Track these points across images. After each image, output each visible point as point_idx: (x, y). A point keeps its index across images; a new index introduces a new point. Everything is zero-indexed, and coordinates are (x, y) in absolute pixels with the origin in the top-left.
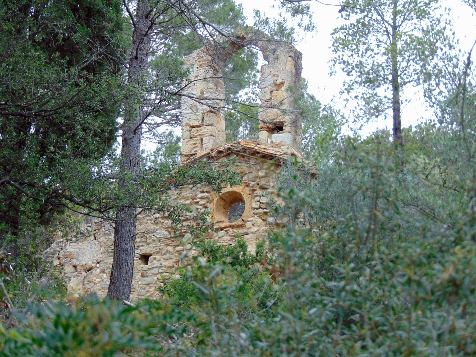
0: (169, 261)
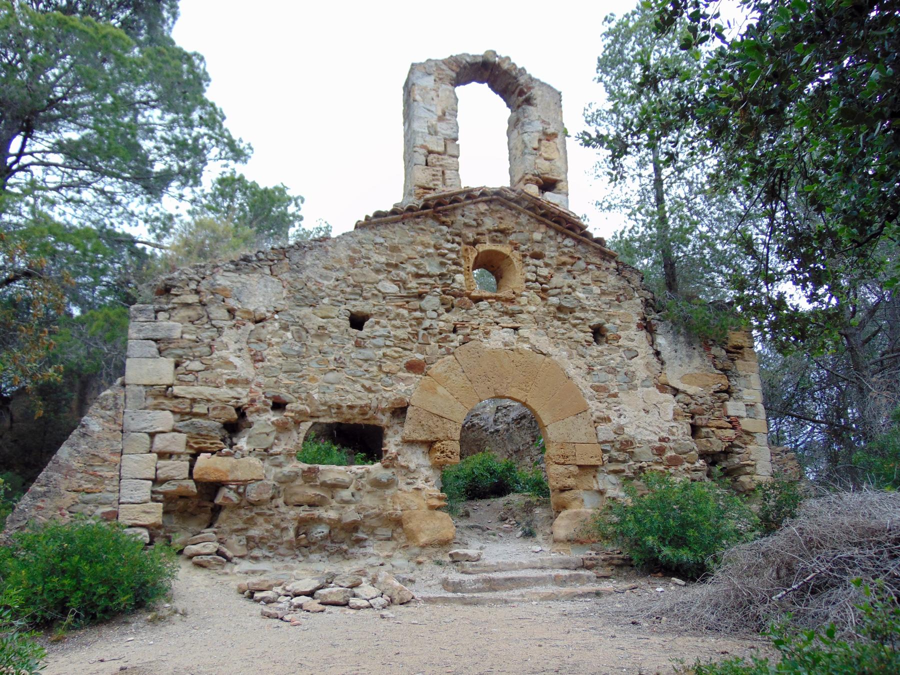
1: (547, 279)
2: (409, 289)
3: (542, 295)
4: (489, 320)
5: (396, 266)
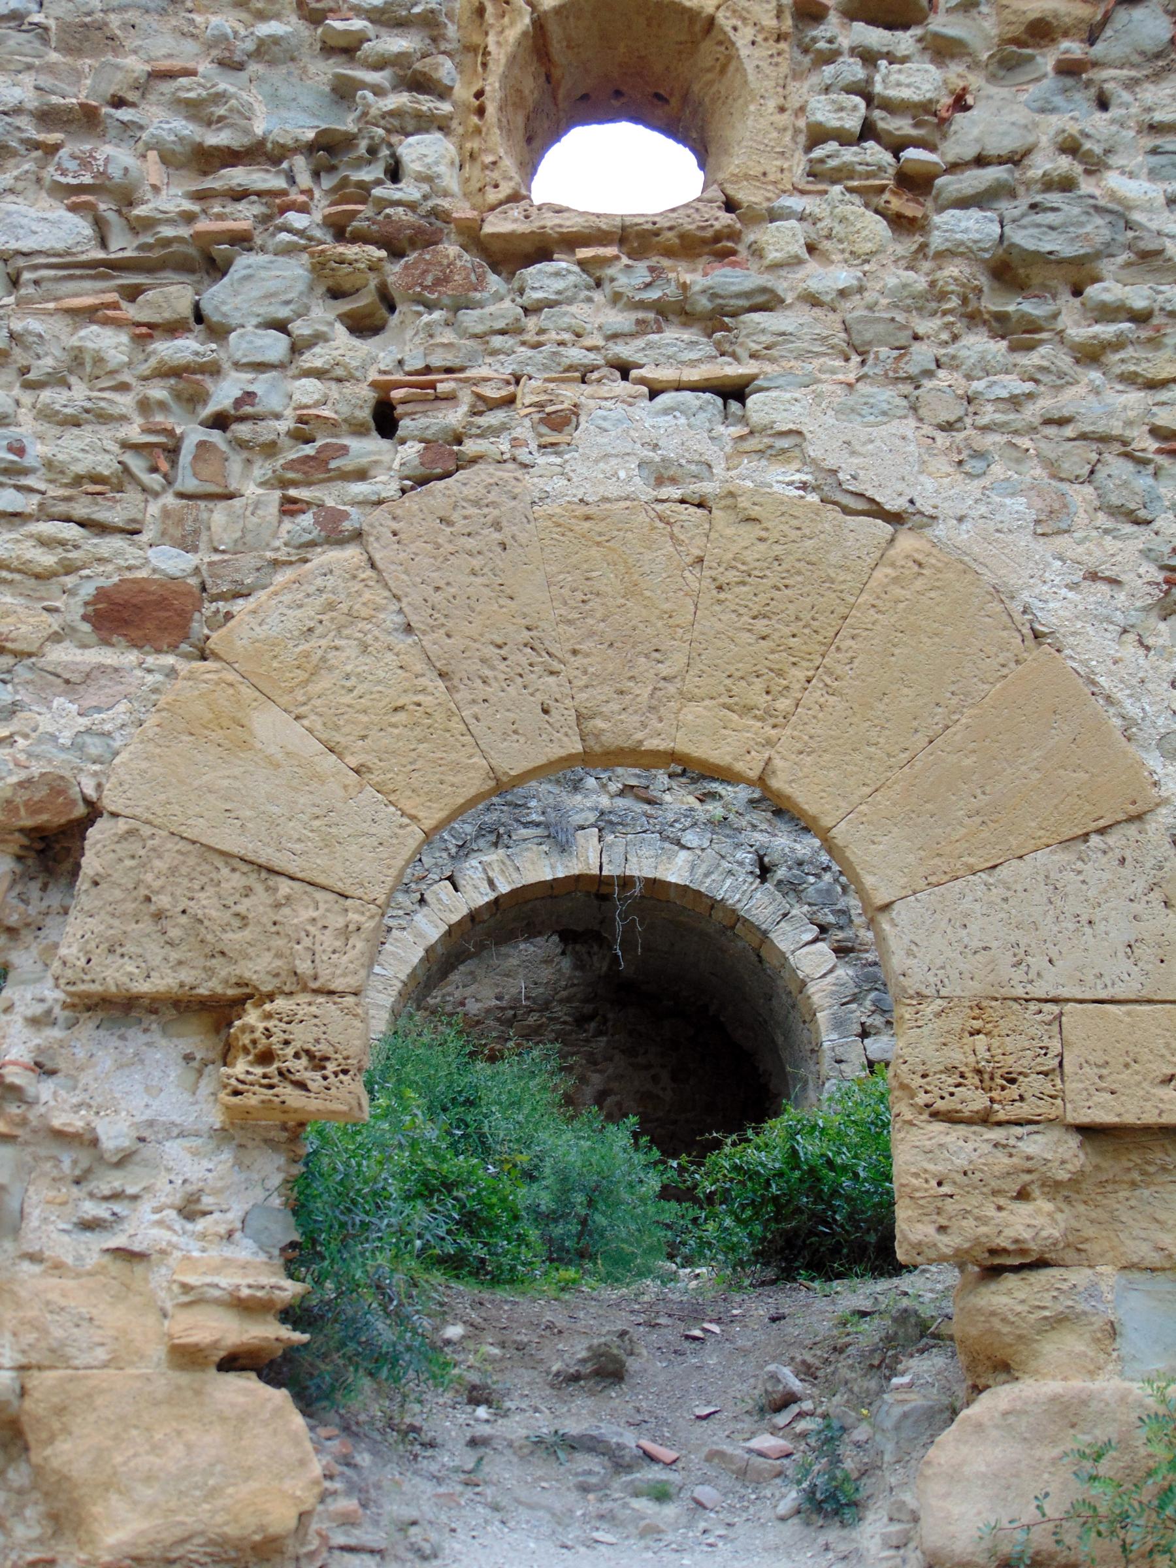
0: (87, 435)
1: (934, 118)
2: (148, 224)
3: (897, 204)
4: (575, 354)
5: (87, 120)
